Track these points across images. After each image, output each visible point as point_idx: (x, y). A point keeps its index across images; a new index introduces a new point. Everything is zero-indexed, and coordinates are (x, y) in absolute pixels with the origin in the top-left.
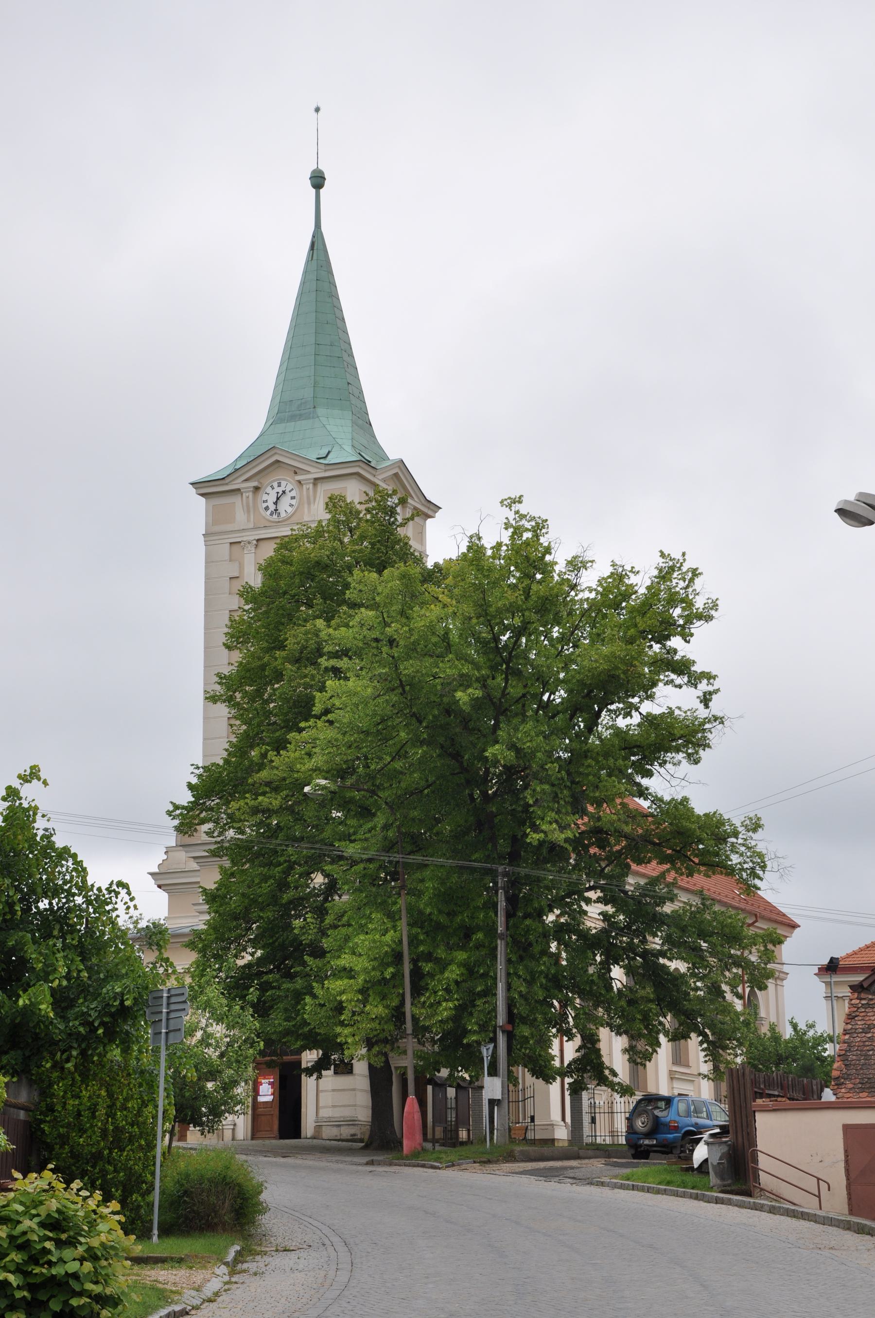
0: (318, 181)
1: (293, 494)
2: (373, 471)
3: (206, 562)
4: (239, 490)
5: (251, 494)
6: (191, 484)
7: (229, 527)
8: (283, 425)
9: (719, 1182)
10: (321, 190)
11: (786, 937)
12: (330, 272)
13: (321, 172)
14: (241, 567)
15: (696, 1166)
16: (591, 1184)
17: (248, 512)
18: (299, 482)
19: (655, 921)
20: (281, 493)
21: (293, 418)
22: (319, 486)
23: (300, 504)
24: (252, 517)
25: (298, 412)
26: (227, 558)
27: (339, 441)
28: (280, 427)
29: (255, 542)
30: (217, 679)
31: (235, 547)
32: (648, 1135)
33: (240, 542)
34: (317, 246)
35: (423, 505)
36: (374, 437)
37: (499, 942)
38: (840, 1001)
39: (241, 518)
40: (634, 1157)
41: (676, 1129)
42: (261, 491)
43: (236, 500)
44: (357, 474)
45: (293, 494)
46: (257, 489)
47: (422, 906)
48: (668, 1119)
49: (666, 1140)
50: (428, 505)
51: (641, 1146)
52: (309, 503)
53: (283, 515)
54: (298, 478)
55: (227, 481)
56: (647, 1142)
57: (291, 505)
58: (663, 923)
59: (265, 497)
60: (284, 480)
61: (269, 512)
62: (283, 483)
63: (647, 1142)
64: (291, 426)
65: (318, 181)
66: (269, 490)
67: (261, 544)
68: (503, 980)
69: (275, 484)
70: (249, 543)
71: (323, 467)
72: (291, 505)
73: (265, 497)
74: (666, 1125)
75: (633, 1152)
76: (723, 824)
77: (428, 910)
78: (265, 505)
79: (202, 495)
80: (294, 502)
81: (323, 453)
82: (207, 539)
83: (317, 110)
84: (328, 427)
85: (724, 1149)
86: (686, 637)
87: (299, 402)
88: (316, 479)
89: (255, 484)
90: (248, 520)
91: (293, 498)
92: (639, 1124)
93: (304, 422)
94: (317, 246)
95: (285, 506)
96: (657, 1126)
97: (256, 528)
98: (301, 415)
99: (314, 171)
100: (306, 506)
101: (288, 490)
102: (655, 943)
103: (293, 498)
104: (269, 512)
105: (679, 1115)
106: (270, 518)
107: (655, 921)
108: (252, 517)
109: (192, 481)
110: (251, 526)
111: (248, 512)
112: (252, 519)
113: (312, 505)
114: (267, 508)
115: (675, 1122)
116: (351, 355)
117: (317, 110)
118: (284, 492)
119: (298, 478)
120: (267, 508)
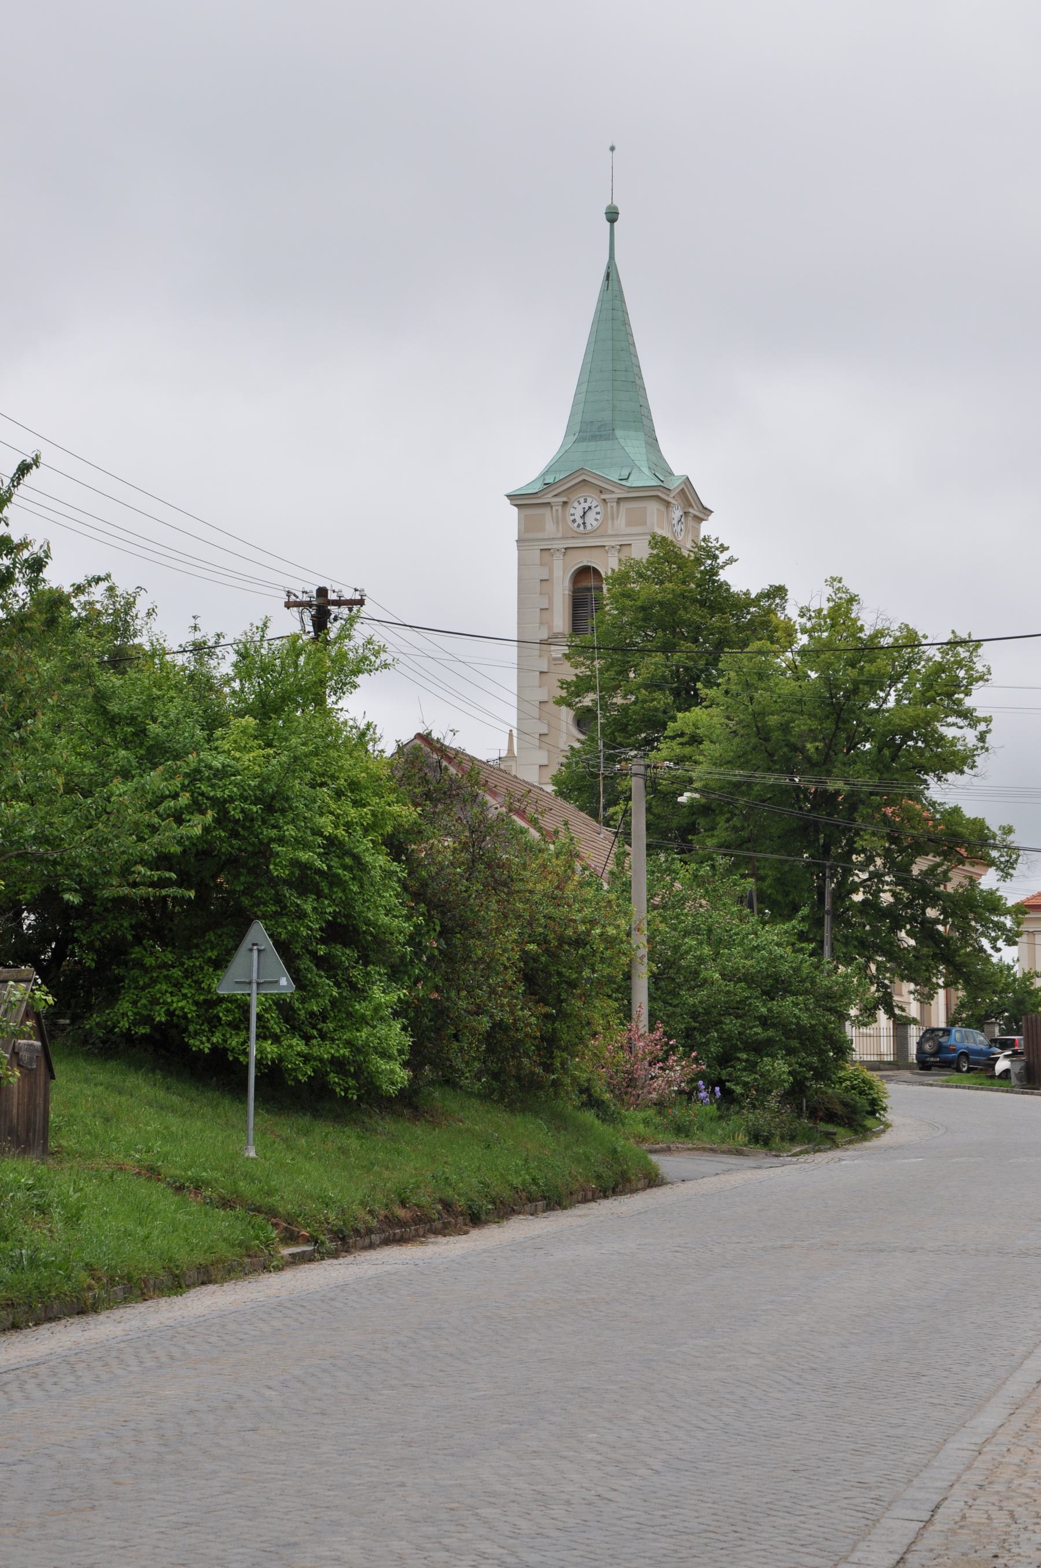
0: (612, 216)
1: (598, 509)
2: (668, 492)
3: (519, 565)
4: (549, 503)
5: (560, 508)
6: (507, 496)
7: (540, 535)
8: (585, 444)
9: (1019, 1083)
10: (615, 224)
11: (981, 875)
12: (623, 301)
13: (616, 208)
14: (551, 571)
15: (997, 1074)
16: (923, 1085)
17: (558, 523)
18: (604, 500)
19: (934, 899)
20: (587, 508)
21: (594, 438)
22: (622, 504)
23: (605, 519)
24: (560, 527)
25: (598, 433)
26: (538, 562)
27: (637, 463)
28: (583, 446)
29: (563, 550)
30: (559, 684)
31: (546, 553)
32: (934, 1054)
33: (550, 549)
34: (611, 276)
35: (700, 512)
36: (659, 451)
37: (826, 916)
38: (1031, 934)
39: (550, 528)
40: (921, 1069)
41: (954, 1051)
42: (569, 505)
43: (546, 511)
44: (657, 497)
45: (598, 509)
46: (565, 503)
47: (765, 888)
48: (949, 1043)
49: (947, 1058)
50: (705, 511)
51: (928, 1062)
52: (613, 519)
53: (589, 527)
54: (603, 496)
55: (539, 495)
56: (932, 1059)
57: (596, 520)
58: (939, 899)
59: (572, 511)
60: (590, 497)
61: (576, 525)
62: (589, 500)
63: (932, 1059)
64: (592, 445)
65: (612, 216)
66: (576, 504)
67: (569, 551)
68: (829, 944)
69: (582, 500)
70: (558, 550)
71: (626, 489)
72: (596, 520)
73: (572, 511)
74: (947, 1048)
75: (921, 1066)
76: (984, 829)
77: (769, 892)
78: (572, 518)
79: (515, 505)
80: (598, 517)
81: (625, 473)
82: (520, 548)
83: (612, 149)
84: (626, 448)
85: (1023, 1064)
86: (968, 693)
87: (599, 424)
88: (619, 499)
89: (565, 499)
90: (558, 530)
91: (598, 513)
92: (927, 1047)
93: (604, 442)
94: (611, 276)
95: (591, 517)
96: (940, 1049)
97: (564, 538)
98: (601, 436)
99: (609, 207)
100: (610, 521)
101: (593, 505)
102: (931, 913)
103: (598, 513)
104: (576, 525)
105: (955, 1040)
106: (576, 529)
107: (934, 899)
108: (560, 527)
109: (509, 491)
110: (560, 535)
111: (558, 523)
112: (561, 530)
113: (615, 521)
114: (574, 521)
115: (954, 1046)
116: (641, 378)
117: (612, 149)
118: (590, 508)
119: (603, 496)
120: (574, 521)
